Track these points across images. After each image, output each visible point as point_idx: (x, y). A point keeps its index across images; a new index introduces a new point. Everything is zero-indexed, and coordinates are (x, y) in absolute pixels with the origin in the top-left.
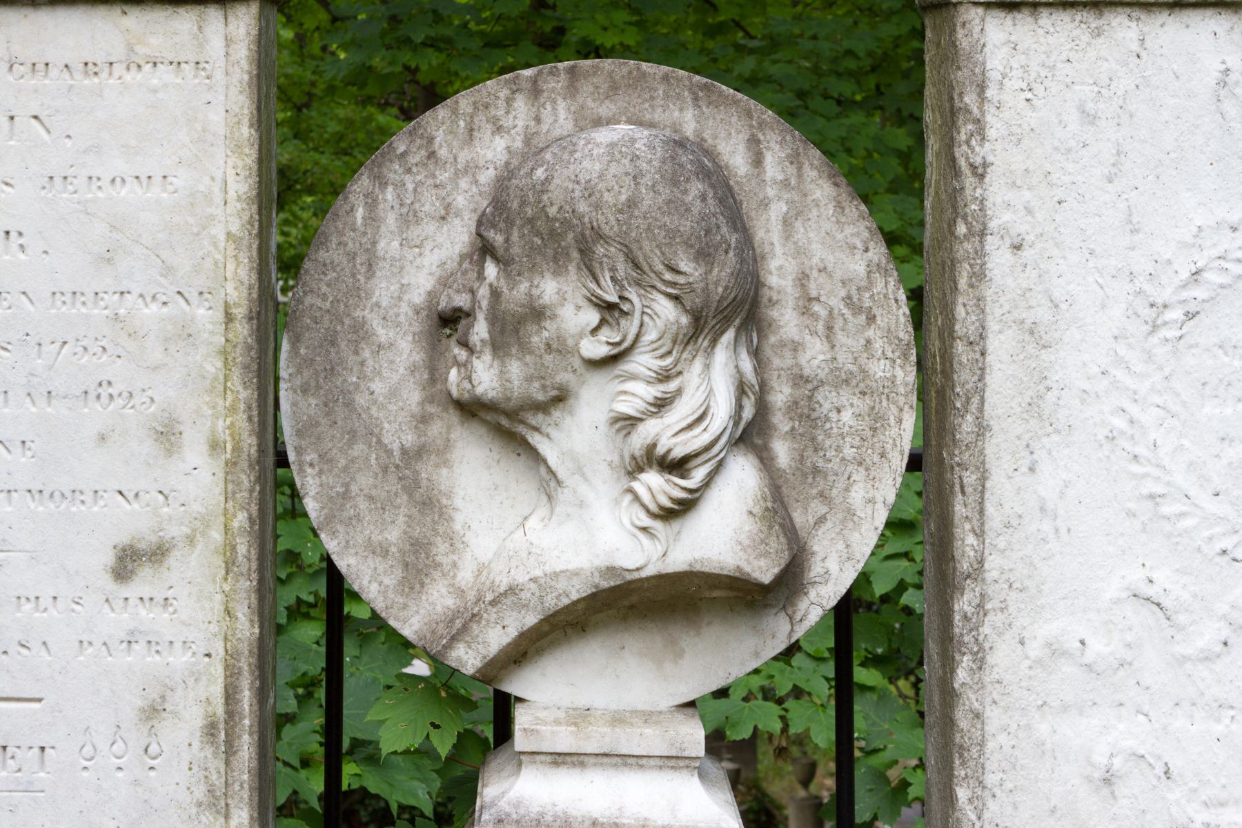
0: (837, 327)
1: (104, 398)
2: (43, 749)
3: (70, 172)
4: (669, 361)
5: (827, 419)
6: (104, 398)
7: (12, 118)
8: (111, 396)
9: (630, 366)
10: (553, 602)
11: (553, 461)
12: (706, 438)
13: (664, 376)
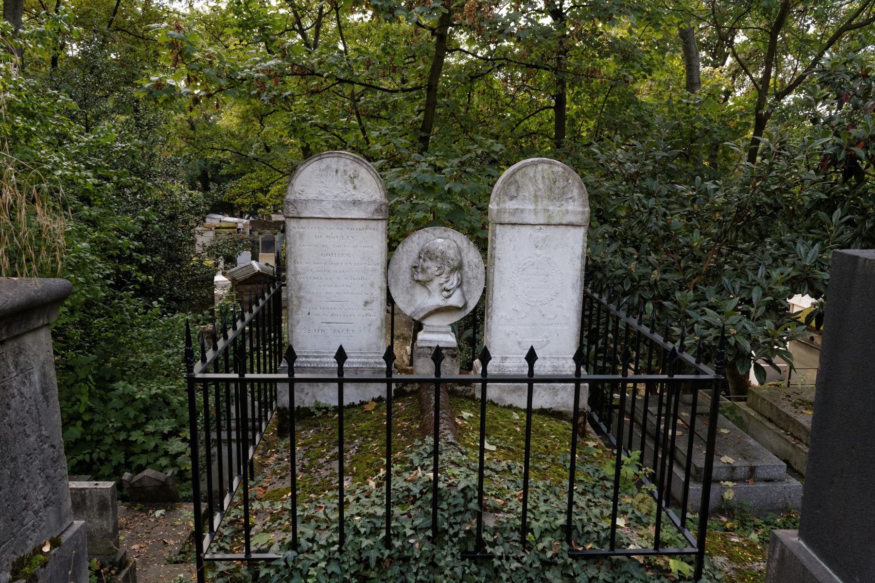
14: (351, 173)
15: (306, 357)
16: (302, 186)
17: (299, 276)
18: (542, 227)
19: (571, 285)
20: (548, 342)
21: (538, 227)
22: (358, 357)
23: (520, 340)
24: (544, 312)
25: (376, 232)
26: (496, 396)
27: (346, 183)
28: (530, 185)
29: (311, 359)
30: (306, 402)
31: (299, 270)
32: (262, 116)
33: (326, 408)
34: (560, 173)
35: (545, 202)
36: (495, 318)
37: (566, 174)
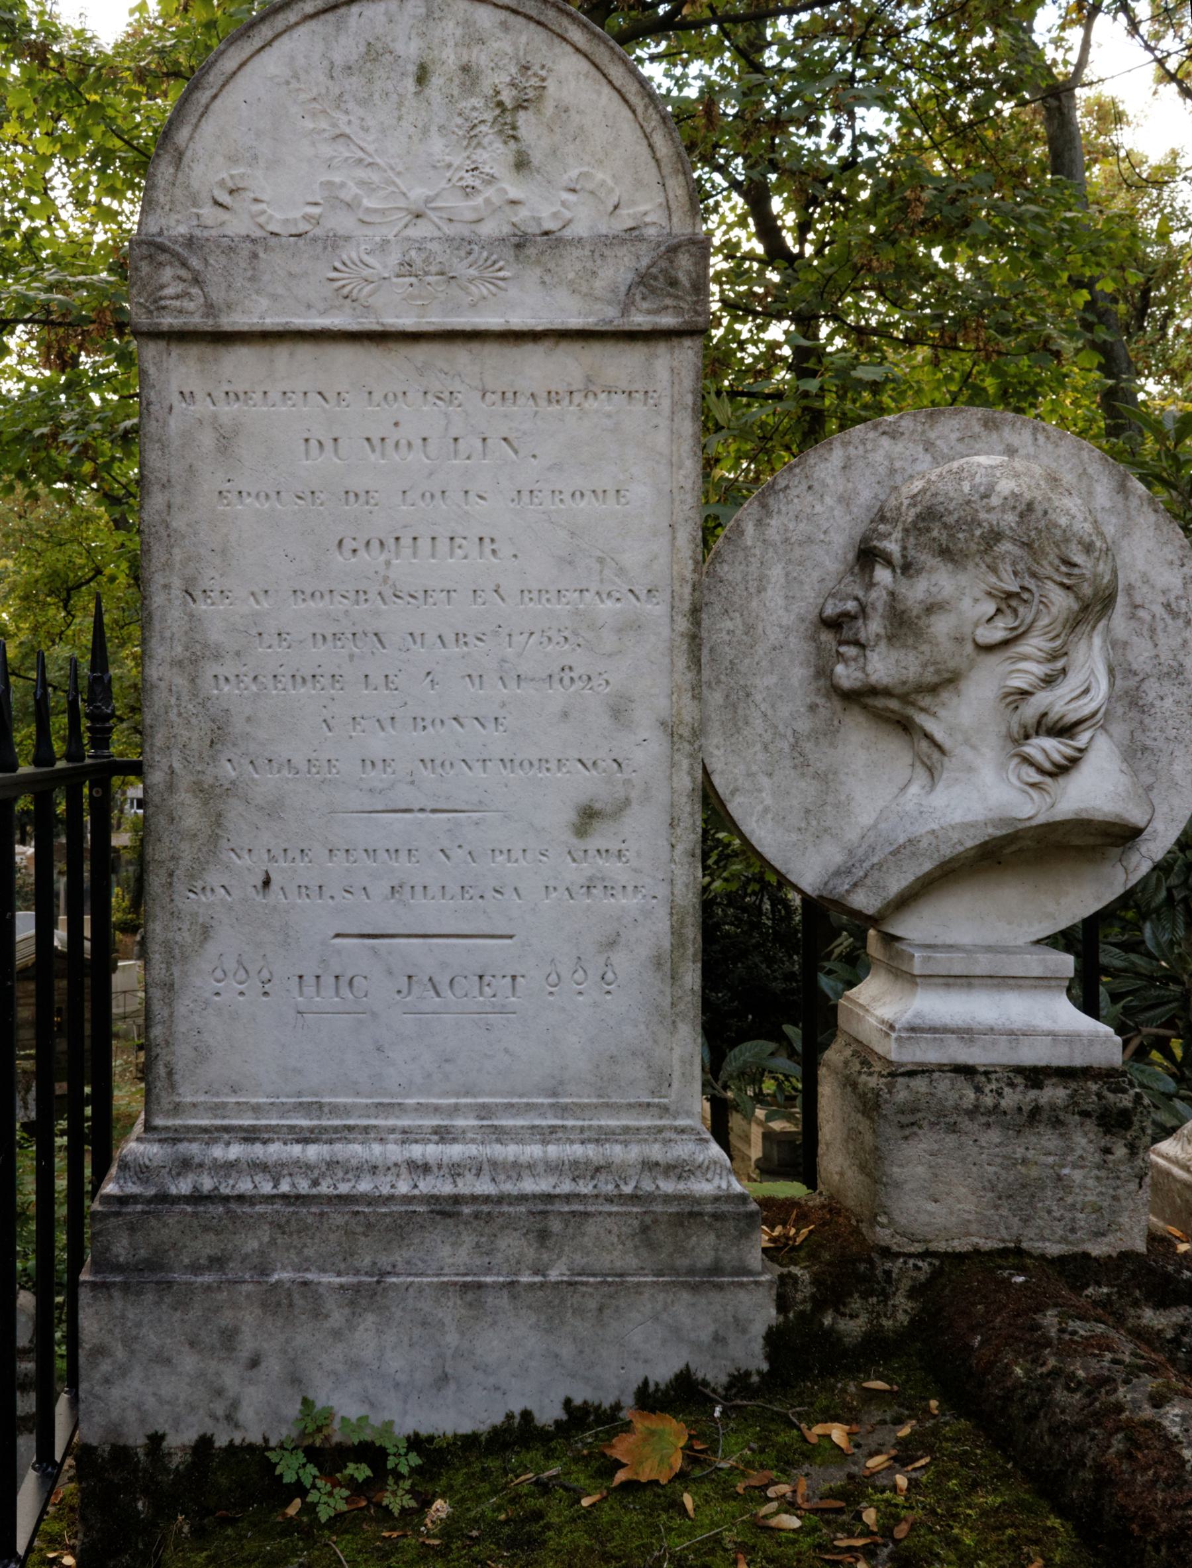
0: (1159, 629)
1: (567, 681)
2: (514, 977)
3: (536, 487)
4: (1058, 643)
5: (1152, 705)
6: (567, 681)
7: (484, 440)
8: (572, 679)
9: (1024, 648)
10: (947, 852)
11: (939, 736)
12: (1093, 706)
13: (1053, 657)
14: (501, 79)
15: (250, 1135)
16: (233, 160)
17: (211, 669)
22: (547, 1135)
25: (638, 408)
27: (472, 138)
29: (275, 1151)
30: (247, 1414)
31: (215, 634)
32: (69, 591)
33: (372, 1453)
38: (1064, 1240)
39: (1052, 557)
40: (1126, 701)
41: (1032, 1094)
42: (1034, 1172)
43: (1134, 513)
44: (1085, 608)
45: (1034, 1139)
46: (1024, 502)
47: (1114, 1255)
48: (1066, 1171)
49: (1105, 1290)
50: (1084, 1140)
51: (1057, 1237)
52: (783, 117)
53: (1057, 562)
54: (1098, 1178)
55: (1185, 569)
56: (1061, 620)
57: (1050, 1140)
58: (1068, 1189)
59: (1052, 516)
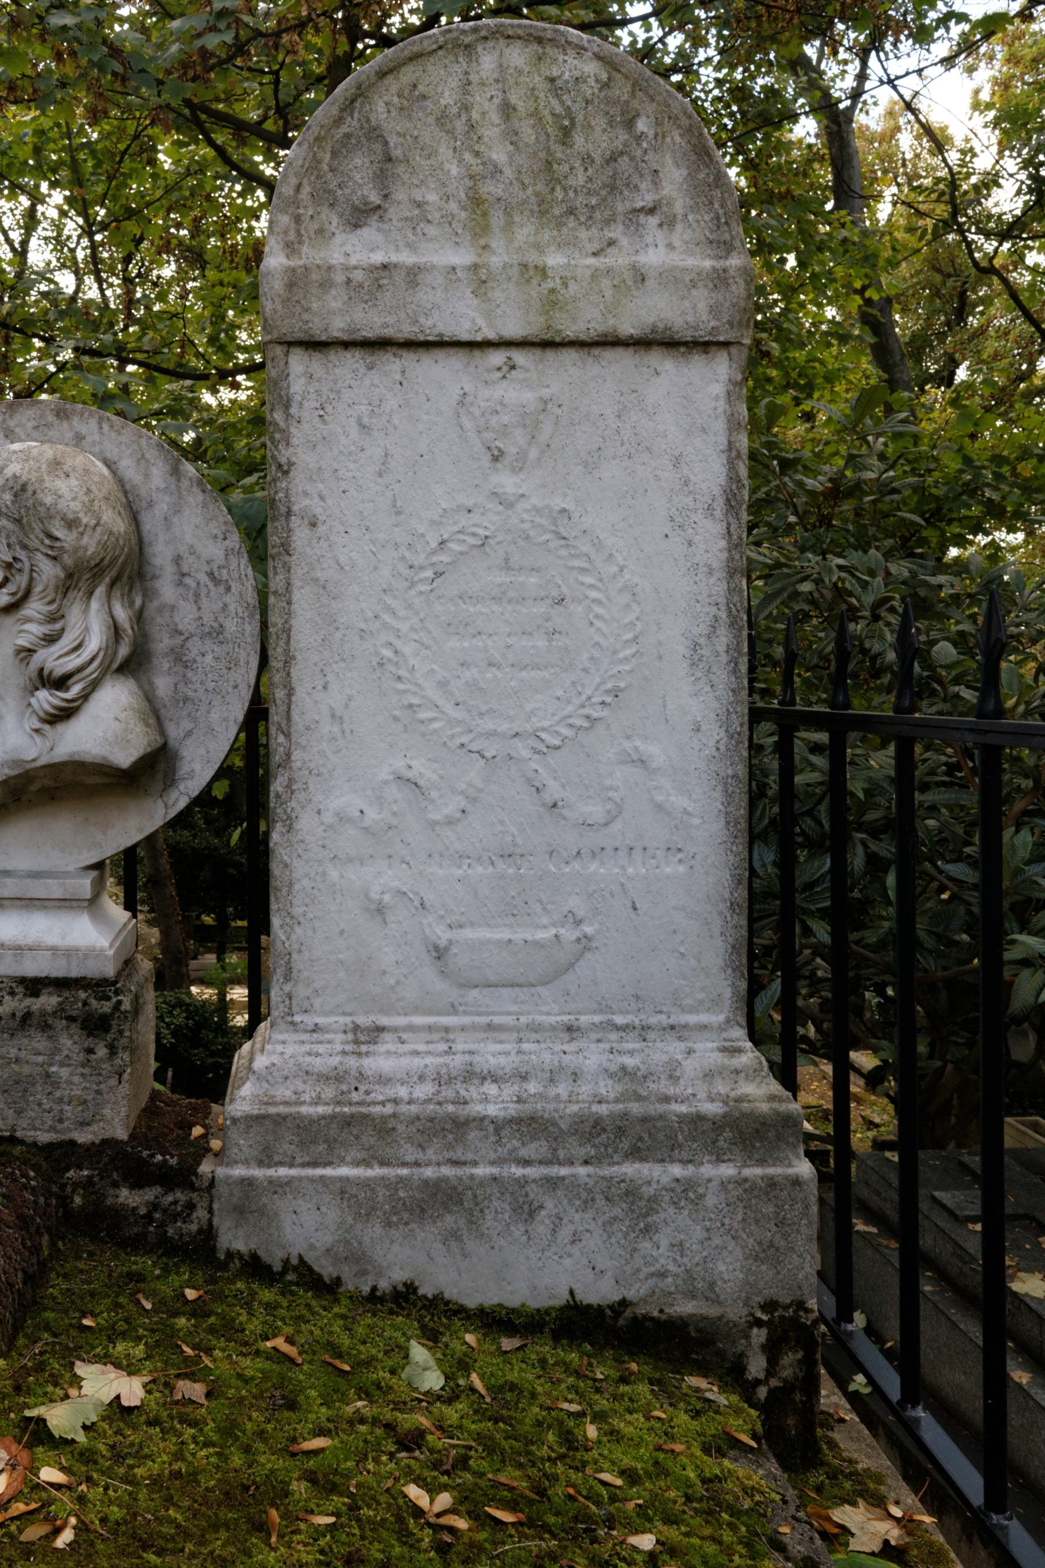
5: (195, 661)
18: (520, 357)
19: (681, 648)
20: (585, 943)
21: (497, 357)
23: (443, 935)
24: (554, 790)
26: (325, 1239)
28: (444, 151)
34: (590, 89)
35: (525, 231)
36: (306, 823)
37: (622, 90)
38: (52, 1129)
39: (37, 531)
40: (172, 658)
41: (28, 1001)
42: (26, 1070)
43: (185, 493)
44: (70, 576)
45: (26, 1041)
46: (20, 482)
47: (97, 1142)
48: (54, 1069)
49: (86, 1173)
50: (69, 1042)
51: (46, 1127)
52: (74, 146)
53: (41, 535)
54: (83, 1075)
55: (227, 542)
56: (51, 586)
57: (40, 1042)
58: (56, 1085)
59: (40, 495)
